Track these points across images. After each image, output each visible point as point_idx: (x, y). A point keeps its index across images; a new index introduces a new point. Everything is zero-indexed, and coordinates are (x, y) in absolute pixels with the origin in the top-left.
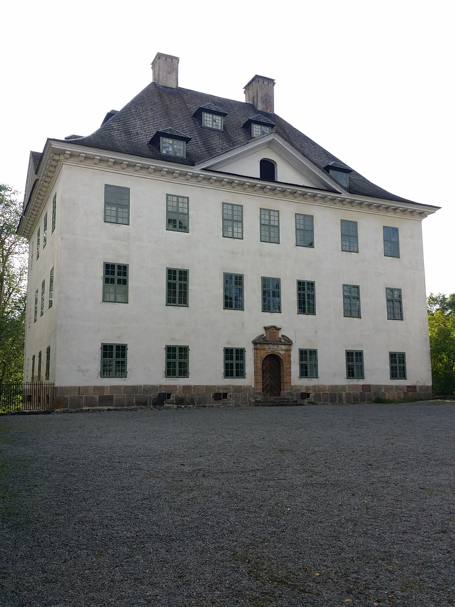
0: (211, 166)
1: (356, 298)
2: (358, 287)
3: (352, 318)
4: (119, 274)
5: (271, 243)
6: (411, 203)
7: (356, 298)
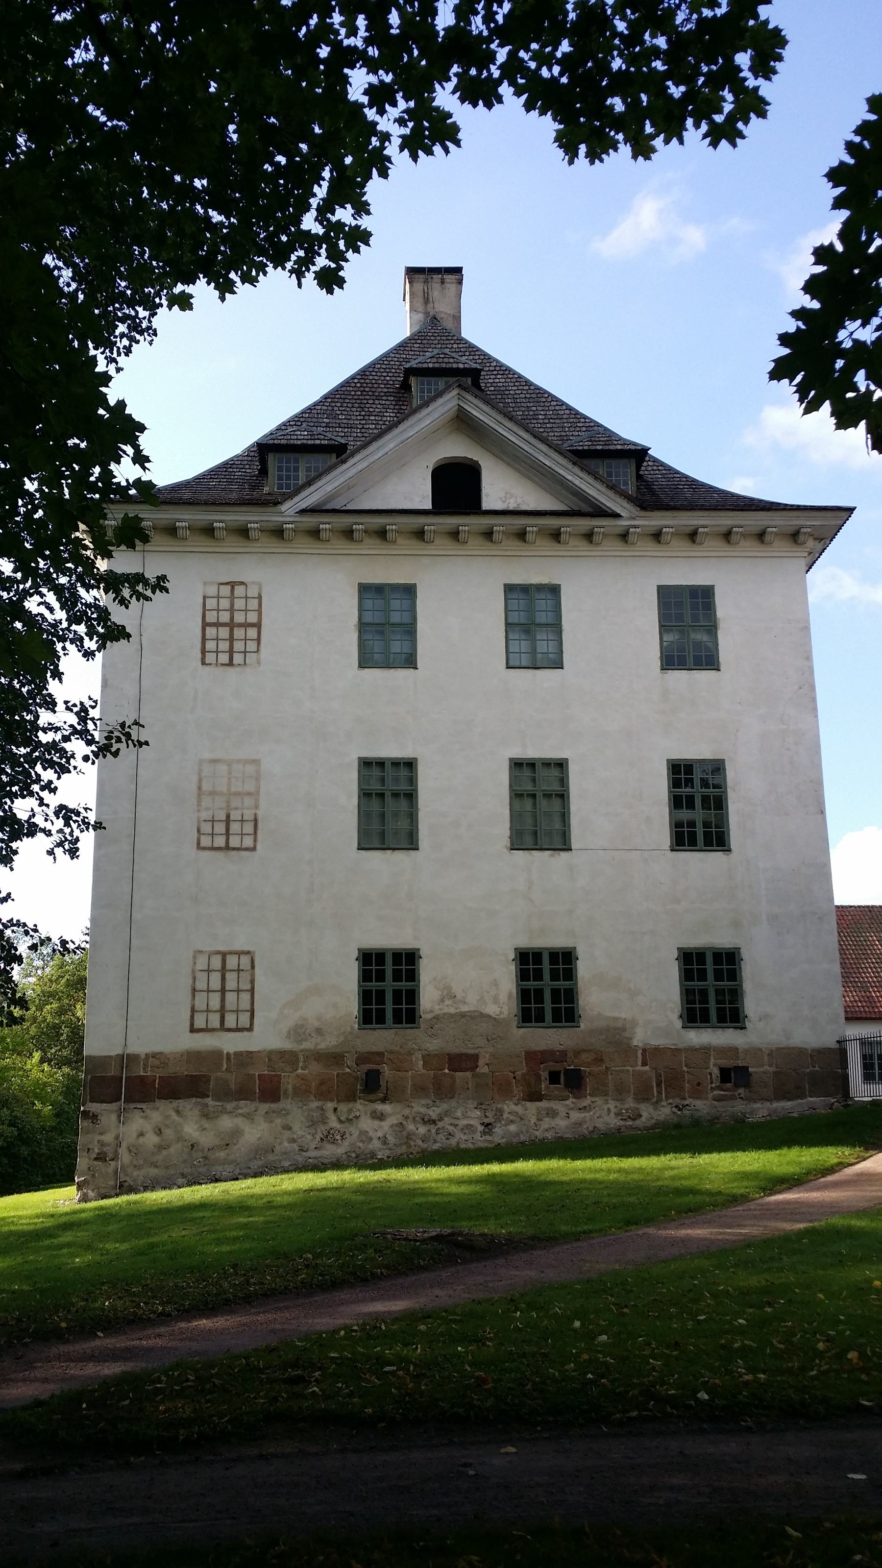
0: (332, 497)
1: (528, 795)
2: (561, 765)
3: (389, 852)
5: (538, 668)
6: (769, 510)
7: (528, 795)
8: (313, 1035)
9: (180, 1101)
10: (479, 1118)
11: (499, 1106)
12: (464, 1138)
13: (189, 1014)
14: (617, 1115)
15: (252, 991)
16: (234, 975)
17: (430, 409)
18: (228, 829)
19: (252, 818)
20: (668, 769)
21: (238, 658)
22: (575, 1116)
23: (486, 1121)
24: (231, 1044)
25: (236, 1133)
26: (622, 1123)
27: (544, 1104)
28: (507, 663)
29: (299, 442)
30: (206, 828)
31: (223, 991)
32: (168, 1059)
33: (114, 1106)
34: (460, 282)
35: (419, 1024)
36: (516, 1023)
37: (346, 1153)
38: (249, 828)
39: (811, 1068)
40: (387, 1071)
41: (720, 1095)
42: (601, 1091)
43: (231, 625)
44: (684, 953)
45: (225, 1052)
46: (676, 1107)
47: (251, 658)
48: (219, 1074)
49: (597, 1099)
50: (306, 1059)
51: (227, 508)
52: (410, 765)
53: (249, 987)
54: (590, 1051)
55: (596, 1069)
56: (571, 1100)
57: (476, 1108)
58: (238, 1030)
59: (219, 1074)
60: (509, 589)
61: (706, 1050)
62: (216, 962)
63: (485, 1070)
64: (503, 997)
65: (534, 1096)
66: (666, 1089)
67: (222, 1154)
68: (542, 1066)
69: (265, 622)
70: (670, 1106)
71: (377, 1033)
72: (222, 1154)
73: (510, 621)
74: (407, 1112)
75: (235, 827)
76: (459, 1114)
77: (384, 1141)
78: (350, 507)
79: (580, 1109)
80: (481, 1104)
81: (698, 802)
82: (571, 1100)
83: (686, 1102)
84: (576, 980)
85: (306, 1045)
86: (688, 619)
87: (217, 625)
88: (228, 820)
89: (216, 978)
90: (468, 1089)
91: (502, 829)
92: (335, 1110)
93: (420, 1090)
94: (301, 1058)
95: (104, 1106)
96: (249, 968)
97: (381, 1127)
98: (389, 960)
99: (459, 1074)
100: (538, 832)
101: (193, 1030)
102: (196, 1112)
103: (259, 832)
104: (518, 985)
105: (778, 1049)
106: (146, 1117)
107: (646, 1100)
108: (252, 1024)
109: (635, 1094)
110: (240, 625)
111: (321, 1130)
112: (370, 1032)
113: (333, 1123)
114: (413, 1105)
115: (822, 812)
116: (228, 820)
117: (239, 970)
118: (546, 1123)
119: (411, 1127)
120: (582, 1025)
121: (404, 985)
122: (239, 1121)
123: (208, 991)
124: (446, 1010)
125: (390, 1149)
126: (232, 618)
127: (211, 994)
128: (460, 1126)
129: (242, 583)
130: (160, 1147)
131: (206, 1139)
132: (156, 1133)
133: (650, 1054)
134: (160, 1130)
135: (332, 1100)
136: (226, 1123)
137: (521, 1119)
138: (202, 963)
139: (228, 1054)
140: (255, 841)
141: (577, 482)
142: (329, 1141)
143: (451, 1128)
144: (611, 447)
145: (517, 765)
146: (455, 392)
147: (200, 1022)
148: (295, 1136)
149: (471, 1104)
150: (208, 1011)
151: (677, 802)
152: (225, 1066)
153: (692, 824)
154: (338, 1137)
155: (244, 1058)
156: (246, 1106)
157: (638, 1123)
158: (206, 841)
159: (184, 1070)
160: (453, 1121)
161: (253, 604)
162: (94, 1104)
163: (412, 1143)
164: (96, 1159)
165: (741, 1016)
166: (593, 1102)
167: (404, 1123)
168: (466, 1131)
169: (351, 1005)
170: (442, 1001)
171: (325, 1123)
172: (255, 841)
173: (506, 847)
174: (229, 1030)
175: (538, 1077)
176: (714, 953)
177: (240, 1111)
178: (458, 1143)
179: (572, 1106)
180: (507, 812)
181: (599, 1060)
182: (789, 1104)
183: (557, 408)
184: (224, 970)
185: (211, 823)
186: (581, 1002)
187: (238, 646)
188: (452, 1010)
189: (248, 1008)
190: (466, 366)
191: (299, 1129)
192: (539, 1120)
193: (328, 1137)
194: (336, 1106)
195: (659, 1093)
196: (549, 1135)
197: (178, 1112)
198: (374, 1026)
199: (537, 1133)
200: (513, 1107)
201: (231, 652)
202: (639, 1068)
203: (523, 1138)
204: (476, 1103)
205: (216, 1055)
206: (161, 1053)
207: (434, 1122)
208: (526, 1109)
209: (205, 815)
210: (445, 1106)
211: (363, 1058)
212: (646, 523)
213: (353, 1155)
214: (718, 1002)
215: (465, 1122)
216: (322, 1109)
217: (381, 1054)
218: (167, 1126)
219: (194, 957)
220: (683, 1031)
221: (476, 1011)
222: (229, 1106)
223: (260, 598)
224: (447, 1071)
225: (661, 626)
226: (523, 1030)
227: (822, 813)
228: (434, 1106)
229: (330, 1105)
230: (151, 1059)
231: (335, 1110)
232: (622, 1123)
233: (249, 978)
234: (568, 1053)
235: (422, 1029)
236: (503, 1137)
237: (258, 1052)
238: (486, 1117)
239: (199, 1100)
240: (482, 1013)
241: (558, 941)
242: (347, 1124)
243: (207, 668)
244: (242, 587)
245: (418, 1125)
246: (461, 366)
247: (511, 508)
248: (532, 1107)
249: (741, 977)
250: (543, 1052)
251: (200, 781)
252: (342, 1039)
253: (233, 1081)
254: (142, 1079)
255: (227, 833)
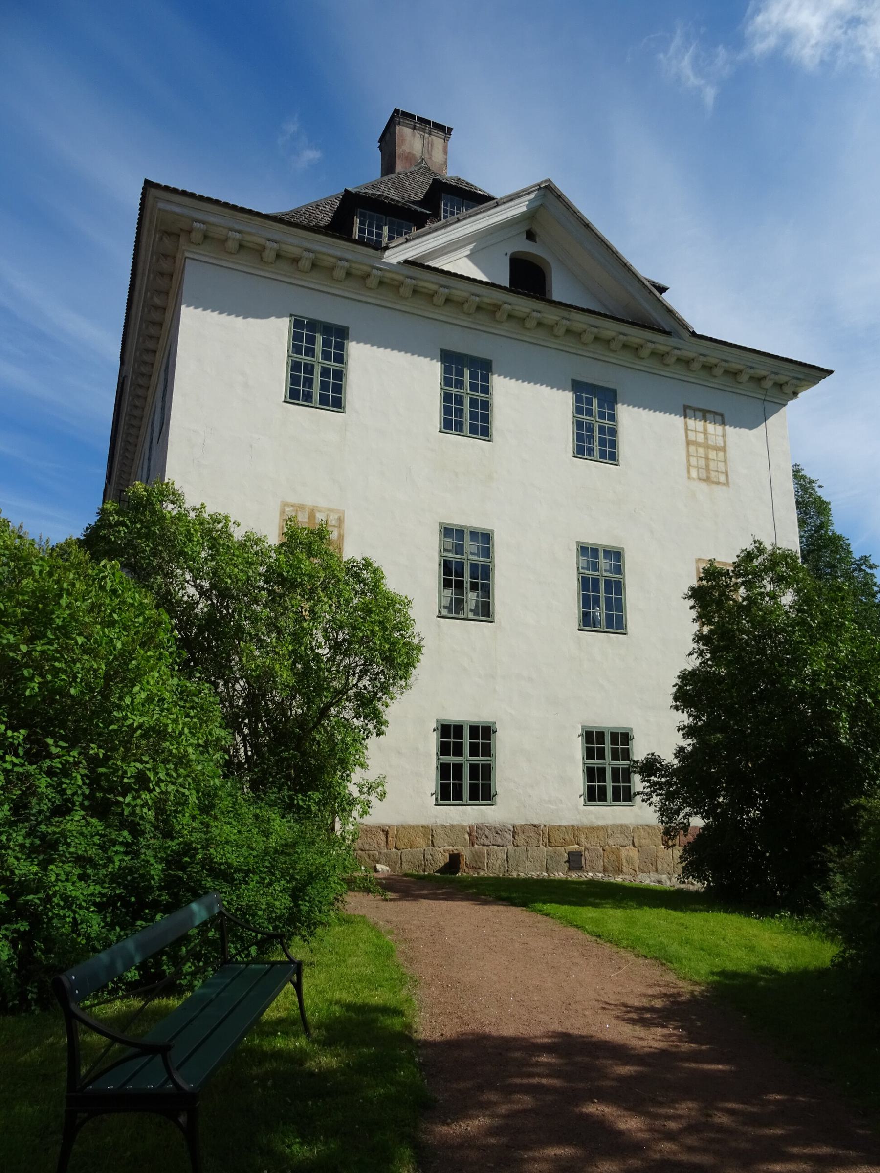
20: (461, 526)
44: (442, 725)
98: (466, 733)
165: (493, 792)
176: (471, 727)
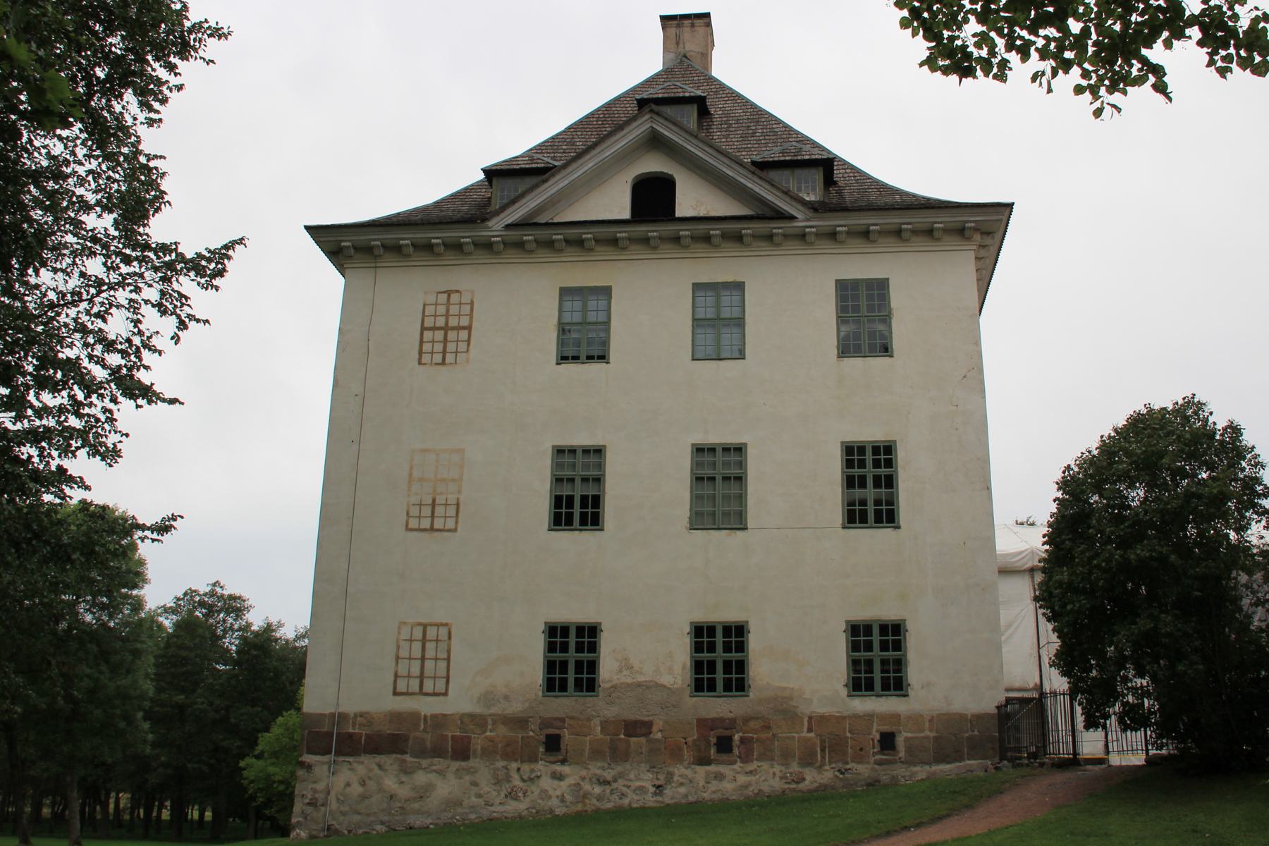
4: (877, 464)
8: (501, 701)
9: (383, 756)
10: (651, 780)
11: (671, 769)
12: (636, 798)
13: (392, 678)
14: (781, 778)
15: (448, 659)
16: (434, 644)
17: (625, 131)
18: (433, 512)
19: (455, 502)
20: (842, 450)
21: (450, 358)
22: (742, 779)
23: (658, 783)
24: (428, 707)
25: (429, 787)
26: (787, 786)
27: (712, 768)
28: (693, 355)
29: (518, 167)
30: (415, 511)
31: (423, 659)
32: (374, 718)
33: (326, 758)
34: (709, 25)
35: (598, 692)
36: (689, 692)
37: (527, 809)
38: (451, 511)
39: (971, 733)
40: (567, 736)
41: (882, 759)
42: (767, 756)
43: (446, 329)
45: (423, 714)
46: (839, 771)
47: (461, 357)
48: (417, 734)
49: (762, 764)
50: (494, 723)
51: (453, 226)
52: (599, 451)
53: (445, 656)
54: (758, 718)
55: (763, 735)
56: (739, 764)
57: (648, 771)
58: (435, 694)
59: (417, 734)
60: (697, 287)
61: (869, 717)
62: (418, 633)
63: (659, 735)
64: (678, 669)
65: (704, 761)
66: (829, 754)
67: (416, 806)
68: (712, 733)
69: (475, 325)
70: (832, 771)
71: (558, 700)
72: (416, 806)
73: (698, 316)
74: (584, 773)
75: (439, 511)
76: (632, 776)
77: (562, 800)
78: (556, 220)
79: (747, 773)
80: (654, 767)
81: (870, 481)
82: (739, 764)
83: (848, 767)
84: (748, 652)
85: (493, 710)
86: (864, 311)
87: (434, 329)
88: (434, 504)
89: (417, 647)
90: (642, 753)
91: (683, 511)
92: (519, 769)
93: (596, 753)
94: (490, 722)
95: (318, 758)
96: (446, 638)
97: (560, 786)
99: (633, 739)
100: (717, 513)
101: (395, 693)
102: (396, 767)
103: (460, 514)
104: (692, 657)
105: (939, 715)
106: (352, 769)
107: (810, 764)
108: (447, 689)
109: (799, 759)
110: (453, 328)
111: (506, 788)
112: (553, 699)
113: (517, 781)
114: (590, 766)
115: (989, 488)
116: (434, 504)
117: (437, 641)
118: (714, 785)
119: (587, 787)
120: (751, 695)
121: (585, 656)
122: (433, 777)
123: (410, 659)
124: (623, 680)
125: (567, 807)
126: (447, 323)
127: (412, 661)
128: (633, 788)
129: (458, 291)
130: (364, 797)
131: (403, 792)
132: (360, 784)
133: (817, 721)
134: (364, 781)
135: (516, 761)
136: (421, 778)
137: (691, 781)
138: (405, 634)
139: (425, 717)
140: (457, 522)
141: (757, 189)
142: (512, 798)
143: (624, 789)
144: (799, 158)
145: (699, 450)
146: (647, 117)
147: (402, 686)
148: (482, 792)
149: (644, 767)
150: (409, 676)
151: (850, 482)
152: (422, 727)
153: (863, 502)
154: (520, 794)
155: (439, 721)
156: (439, 763)
157: (801, 786)
158: (413, 523)
159: (388, 729)
160: (626, 783)
161: (466, 309)
162: (310, 756)
163: (587, 801)
164: (309, 804)
166: (759, 767)
167: (582, 783)
168: (638, 792)
169: (536, 673)
170: (621, 671)
171: (509, 781)
172: (457, 522)
173: (686, 527)
174: (427, 694)
175: (708, 743)
177: (434, 768)
178: (630, 804)
179: (739, 770)
180: (688, 495)
181: (767, 727)
182: (948, 767)
183: (774, 126)
184: (424, 640)
185: (418, 507)
186: (751, 673)
187: (451, 347)
188: (629, 680)
189: (444, 674)
190: (692, 94)
191: (486, 787)
192: (708, 783)
193: (511, 795)
194: (519, 766)
195: (823, 757)
196: (715, 796)
197: (380, 767)
198: (557, 693)
199: (705, 795)
200: (683, 771)
201: (444, 352)
202: (805, 734)
203: (691, 799)
204: (648, 766)
205: (414, 717)
206: (367, 713)
207: (608, 783)
208: (695, 773)
209: (414, 499)
210: (619, 769)
211: (545, 723)
212: (821, 223)
213: (534, 811)
214: (882, 671)
215: (638, 784)
216: (507, 769)
217: (562, 720)
218: (370, 778)
219: (399, 628)
220: (848, 699)
221: (651, 681)
222: (425, 763)
223: (472, 303)
224: (622, 736)
225: (838, 317)
226: (694, 699)
227: (988, 489)
228: (609, 768)
229: (514, 765)
230: (359, 719)
231: (519, 769)
232: (787, 786)
233: (446, 648)
234: (738, 722)
235: (600, 697)
236: (672, 798)
237: (452, 715)
238: (658, 779)
239: (399, 756)
240: (656, 683)
241: (730, 615)
242: (529, 783)
243: (422, 367)
244: (458, 294)
245: (594, 786)
246: (687, 95)
247: (702, 215)
248: (701, 770)
249: (906, 647)
250: (713, 720)
251: (411, 468)
252: (527, 705)
253: (429, 739)
254: (350, 735)
255: (433, 516)
